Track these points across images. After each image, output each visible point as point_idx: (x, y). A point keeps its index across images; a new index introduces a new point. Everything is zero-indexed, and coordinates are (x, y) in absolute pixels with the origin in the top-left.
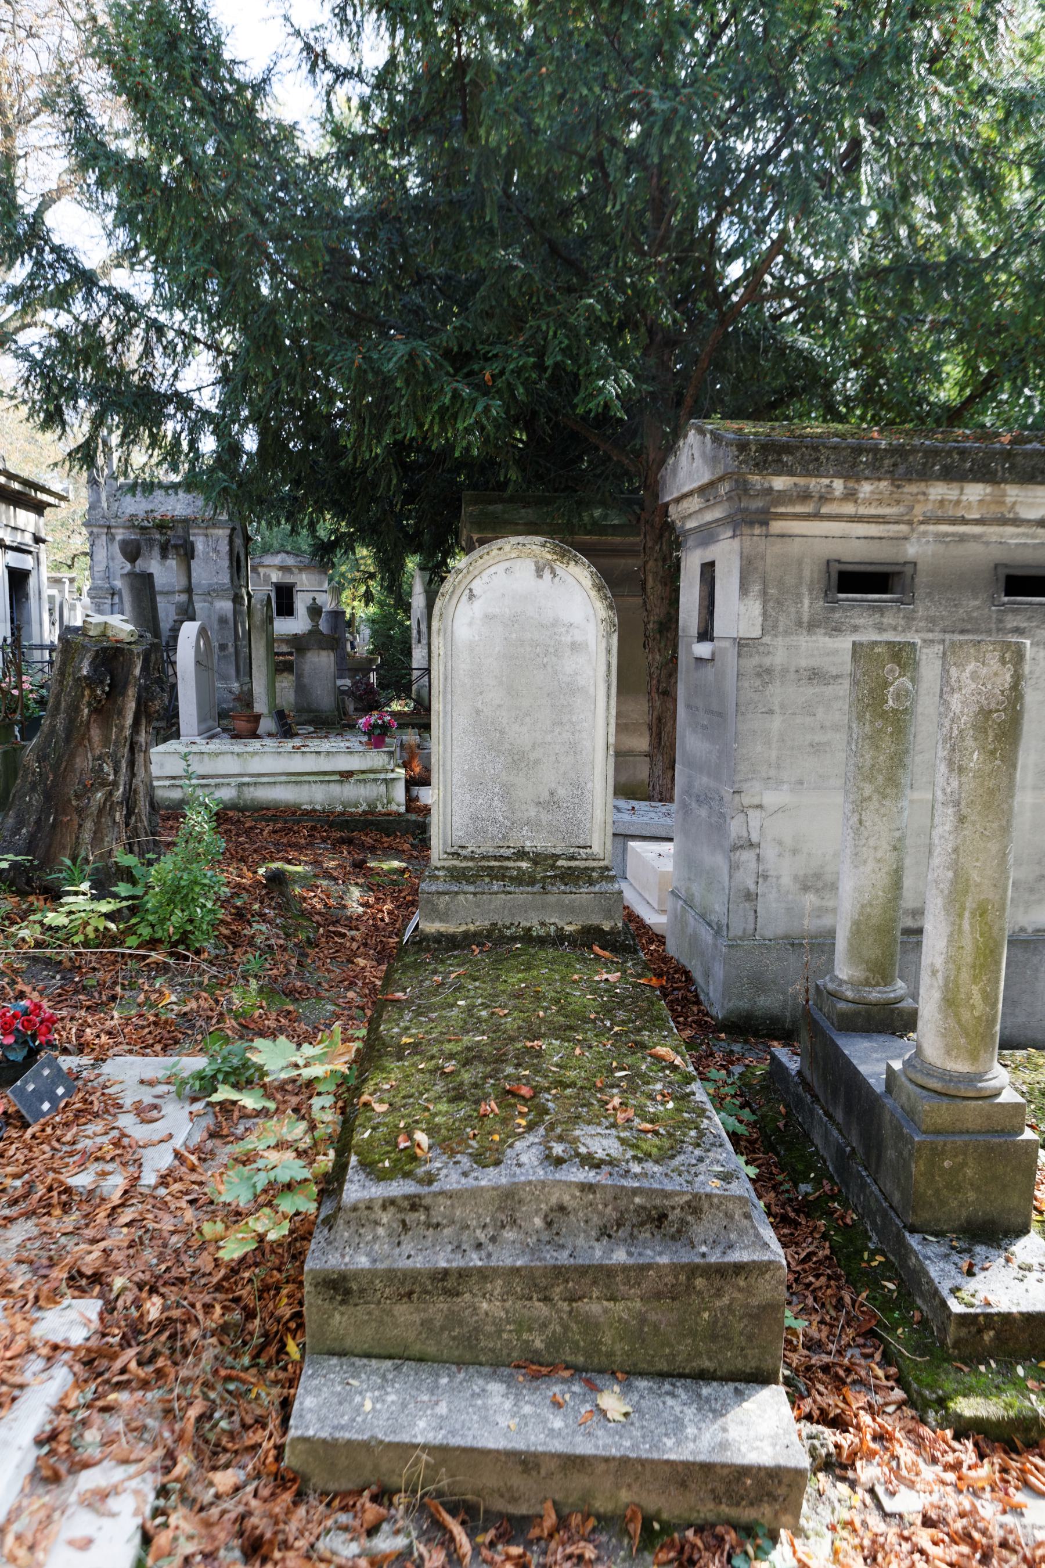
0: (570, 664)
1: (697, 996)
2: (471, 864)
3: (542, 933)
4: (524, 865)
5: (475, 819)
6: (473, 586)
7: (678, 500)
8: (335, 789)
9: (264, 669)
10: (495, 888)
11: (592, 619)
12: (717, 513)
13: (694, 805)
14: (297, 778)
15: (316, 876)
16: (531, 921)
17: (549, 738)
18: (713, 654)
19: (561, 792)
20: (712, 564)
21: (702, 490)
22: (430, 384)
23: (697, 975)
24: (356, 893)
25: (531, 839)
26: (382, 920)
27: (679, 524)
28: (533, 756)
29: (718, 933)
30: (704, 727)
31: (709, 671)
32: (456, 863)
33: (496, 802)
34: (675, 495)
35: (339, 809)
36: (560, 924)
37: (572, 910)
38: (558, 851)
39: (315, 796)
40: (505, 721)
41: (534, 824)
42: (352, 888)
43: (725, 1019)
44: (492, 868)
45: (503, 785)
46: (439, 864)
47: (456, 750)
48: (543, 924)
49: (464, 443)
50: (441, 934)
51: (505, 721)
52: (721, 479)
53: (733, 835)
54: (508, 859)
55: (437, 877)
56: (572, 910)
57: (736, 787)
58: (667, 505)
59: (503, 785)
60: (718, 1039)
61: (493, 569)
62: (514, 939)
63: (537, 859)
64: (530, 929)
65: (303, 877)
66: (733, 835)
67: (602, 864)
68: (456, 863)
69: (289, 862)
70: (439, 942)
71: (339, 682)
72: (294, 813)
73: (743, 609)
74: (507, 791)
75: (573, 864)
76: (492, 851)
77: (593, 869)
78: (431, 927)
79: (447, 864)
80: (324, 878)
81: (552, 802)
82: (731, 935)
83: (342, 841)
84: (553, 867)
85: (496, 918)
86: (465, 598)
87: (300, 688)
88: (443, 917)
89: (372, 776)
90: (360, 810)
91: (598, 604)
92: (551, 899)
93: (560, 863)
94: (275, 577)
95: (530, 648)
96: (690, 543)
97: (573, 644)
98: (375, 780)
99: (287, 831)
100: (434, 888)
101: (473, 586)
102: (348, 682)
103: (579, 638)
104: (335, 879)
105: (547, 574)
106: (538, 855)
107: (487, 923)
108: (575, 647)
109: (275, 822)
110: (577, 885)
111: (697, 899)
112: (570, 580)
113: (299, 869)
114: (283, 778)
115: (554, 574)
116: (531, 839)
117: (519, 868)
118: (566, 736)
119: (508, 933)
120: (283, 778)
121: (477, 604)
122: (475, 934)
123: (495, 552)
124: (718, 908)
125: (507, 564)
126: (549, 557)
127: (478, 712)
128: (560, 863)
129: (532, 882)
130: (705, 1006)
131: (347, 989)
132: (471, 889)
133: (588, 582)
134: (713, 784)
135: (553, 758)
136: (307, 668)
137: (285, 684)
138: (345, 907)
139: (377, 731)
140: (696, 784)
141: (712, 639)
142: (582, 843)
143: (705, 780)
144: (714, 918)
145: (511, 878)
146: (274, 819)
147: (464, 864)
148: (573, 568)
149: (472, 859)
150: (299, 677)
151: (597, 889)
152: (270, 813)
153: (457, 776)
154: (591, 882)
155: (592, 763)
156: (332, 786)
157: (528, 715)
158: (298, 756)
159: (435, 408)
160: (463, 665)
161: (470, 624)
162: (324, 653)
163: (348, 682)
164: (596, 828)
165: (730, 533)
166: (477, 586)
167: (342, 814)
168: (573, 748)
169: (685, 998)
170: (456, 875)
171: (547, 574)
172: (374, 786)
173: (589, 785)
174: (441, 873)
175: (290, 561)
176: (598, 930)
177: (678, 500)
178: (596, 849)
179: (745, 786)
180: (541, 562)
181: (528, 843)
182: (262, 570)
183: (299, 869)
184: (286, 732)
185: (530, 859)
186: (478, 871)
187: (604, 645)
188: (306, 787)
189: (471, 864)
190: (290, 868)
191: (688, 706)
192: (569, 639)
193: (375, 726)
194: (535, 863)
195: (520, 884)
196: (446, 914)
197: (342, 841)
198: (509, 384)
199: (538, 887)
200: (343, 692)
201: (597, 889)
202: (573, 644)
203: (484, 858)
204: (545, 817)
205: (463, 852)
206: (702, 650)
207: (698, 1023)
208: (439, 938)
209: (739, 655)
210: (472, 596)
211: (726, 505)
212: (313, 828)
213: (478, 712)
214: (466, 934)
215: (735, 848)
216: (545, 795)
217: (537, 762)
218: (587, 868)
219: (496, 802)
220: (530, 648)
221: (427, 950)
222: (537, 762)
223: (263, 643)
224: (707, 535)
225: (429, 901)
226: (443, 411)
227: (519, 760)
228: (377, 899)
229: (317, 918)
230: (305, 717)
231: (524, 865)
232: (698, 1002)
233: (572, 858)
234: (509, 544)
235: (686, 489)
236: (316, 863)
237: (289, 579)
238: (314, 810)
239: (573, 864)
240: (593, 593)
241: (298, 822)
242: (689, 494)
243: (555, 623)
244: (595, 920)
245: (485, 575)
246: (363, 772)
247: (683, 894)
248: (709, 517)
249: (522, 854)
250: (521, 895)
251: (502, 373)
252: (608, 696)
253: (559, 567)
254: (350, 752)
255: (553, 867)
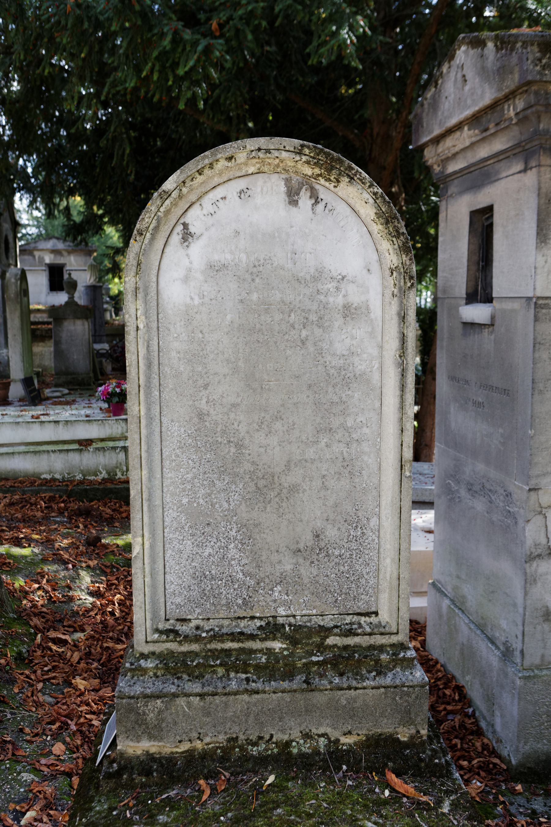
0: (343, 339)
1: (476, 723)
2: (195, 647)
3: (306, 748)
4: (277, 645)
5: (200, 577)
6: (189, 218)
7: (437, 140)
8: (75, 458)
9: (19, 338)
10: (233, 685)
11: (375, 267)
12: (499, 145)
13: (463, 493)
14: (35, 448)
15: (44, 560)
16: (290, 732)
17: (310, 453)
18: (493, 318)
19: (331, 533)
20: (489, 210)
21: (475, 120)
22: (150, 29)
23: (475, 693)
24: (86, 578)
25: (287, 604)
26: (112, 613)
27: (437, 169)
28: (288, 480)
29: (507, 654)
30: (480, 405)
31: (487, 339)
32: (173, 646)
33: (233, 552)
34: (437, 131)
35: (79, 477)
36: (334, 734)
37: (351, 713)
38: (327, 622)
39: (54, 466)
40: (243, 429)
41: (290, 583)
42: (83, 573)
43: (521, 764)
44: (228, 652)
45: (242, 526)
46: (146, 649)
47: (169, 474)
48: (307, 736)
49: (189, 94)
50: (151, 757)
51: (243, 429)
52: (509, 97)
53: (529, 542)
54: (252, 637)
55: (144, 671)
56: (351, 713)
57: (533, 483)
58: (421, 149)
59: (242, 526)
60: (514, 792)
61: (219, 192)
62: (263, 762)
63: (297, 635)
64: (288, 744)
65: (31, 562)
66: (529, 542)
67: (394, 639)
68: (173, 646)
69: (17, 542)
70: (148, 773)
71: (97, 346)
72: (32, 483)
73: (541, 260)
74: (248, 534)
75: (351, 641)
76: (227, 626)
77: (381, 648)
78: (135, 747)
79: (158, 648)
80: (54, 562)
81: (317, 548)
82: (527, 663)
83: (80, 513)
84: (321, 647)
85: (235, 730)
86: (176, 238)
87: (59, 353)
88: (154, 732)
89: (111, 444)
90: (100, 478)
91: (386, 245)
92: (319, 698)
93: (331, 641)
94: (48, 259)
95: (282, 312)
96: (453, 189)
97: (347, 307)
98: (114, 448)
99: (24, 503)
100: (138, 689)
101: (189, 218)
102: (106, 346)
103: (355, 299)
104: (65, 563)
105: (305, 200)
106: (298, 628)
107: (222, 738)
108: (349, 312)
109: (13, 493)
110: (357, 674)
111: (471, 603)
112: (342, 208)
113: (26, 552)
114: (22, 448)
115: (316, 199)
116: (287, 604)
117: (269, 652)
118: (338, 448)
119: (254, 751)
120: (22, 448)
121: (196, 248)
122: (205, 755)
123: (222, 164)
124: (506, 626)
125: (241, 184)
126: (308, 171)
127: (201, 416)
128: (331, 641)
129: (289, 674)
130: (489, 738)
131: (56, 737)
132: (197, 687)
133: (369, 211)
134: (493, 474)
135: (318, 483)
136: (64, 335)
137: (44, 351)
138: (71, 599)
139: (115, 400)
140: (468, 470)
141: (488, 299)
142: (362, 607)
143: (481, 467)
144: (500, 637)
145: (258, 667)
146: (11, 490)
147: (185, 648)
148: (347, 189)
149: (197, 639)
150: (57, 344)
151: (388, 680)
152: (9, 483)
153: (171, 514)
154: (380, 670)
155: (378, 488)
156: (71, 455)
157: (278, 418)
158: (36, 427)
159: (155, 54)
160: (176, 343)
161: (186, 279)
162: (79, 322)
163: (106, 346)
164: (384, 585)
165: (520, 166)
166: (196, 218)
167: (81, 482)
168: (348, 467)
169: (462, 725)
170: (174, 666)
171: (305, 200)
172: (113, 454)
173: (374, 522)
174: (149, 664)
175: (60, 245)
176: (391, 740)
177: (437, 140)
178: (385, 616)
179: (544, 482)
180: (296, 179)
181: (282, 611)
182: (37, 254)
183: (26, 552)
184: (34, 397)
185: (285, 637)
186: (208, 657)
187: (394, 308)
188: (45, 456)
189: (195, 647)
190: (16, 551)
191: (452, 378)
192: (340, 300)
193: (113, 394)
194: (294, 642)
195: (272, 677)
196: (158, 727)
197: (80, 513)
198: (237, 30)
199: (298, 681)
200: (103, 355)
201: (388, 680)
202: (347, 307)
203: (217, 637)
204: (307, 572)
205: (183, 629)
206: (477, 313)
207: (485, 767)
208: (148, 764)
209: (536, 319)
210: (187, 236)
211: (515, 131)
212: (52, 499)
213: (201, 416)
214: (190, 755)
215: (531, 558)
216: (307, 539)
217: (294, 489)
218: (372, 647)
219: (233, 552)
220: (282, 312)
221: (130, 786)
222: (294, 489)
223: (18, 313)
224: (480, 175)
225: (130, 710)
226: (164, 54)
227: (266, 487)
228: (109, 586)
229: (36, 621)
230: (63, 379)
231: (277, 645)
232: (479, 733)
233: (350, 633)
234: (244, 149)
235: (453, 121)
236: (48, 542)
237: (60, 260)
238: (54, 480)
239: (351, 641)
240: (377, 228)
241: (37, 492)
242: (459, 127)
243: (319, 275)
244: (386, 727)
245: (207, 201)
246: (102, 440)
247: (449, 590)
248: (483, 152)
249: (272, 629)
250: (274, 695)
251: (230, 18)
252: (403, 388)
253: (324, 188)
254: (89, 420)
255: (321, 647)
